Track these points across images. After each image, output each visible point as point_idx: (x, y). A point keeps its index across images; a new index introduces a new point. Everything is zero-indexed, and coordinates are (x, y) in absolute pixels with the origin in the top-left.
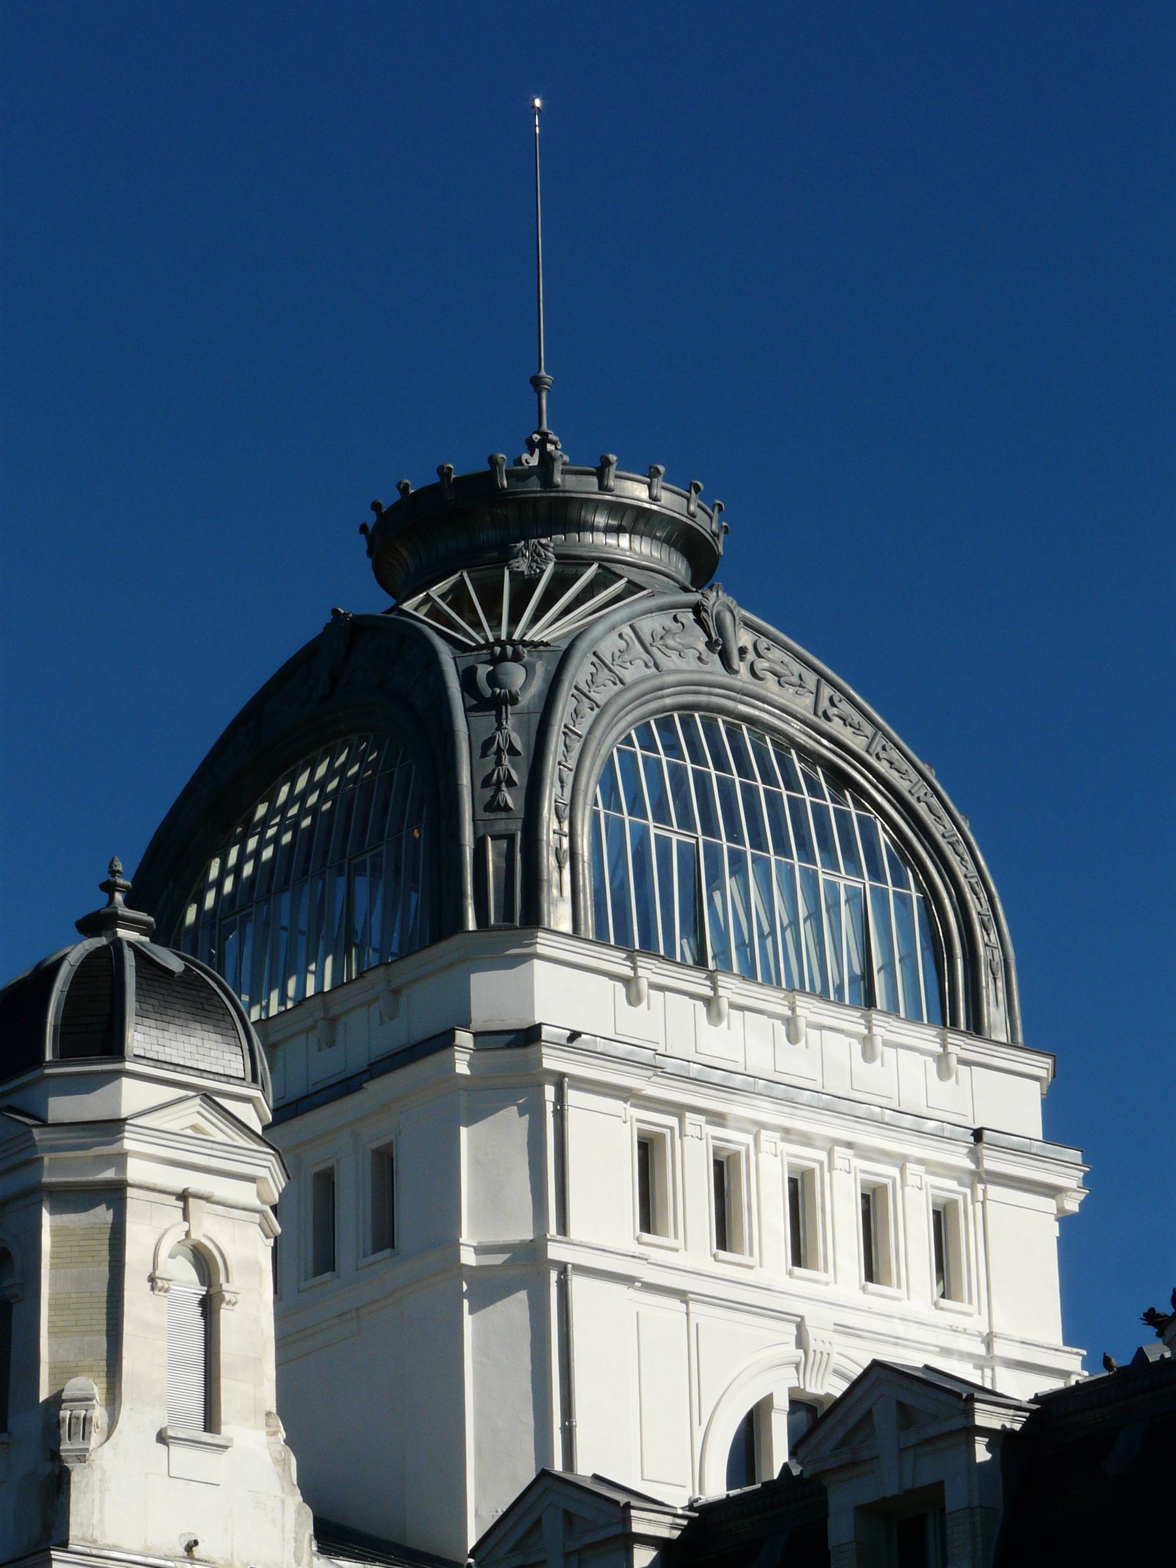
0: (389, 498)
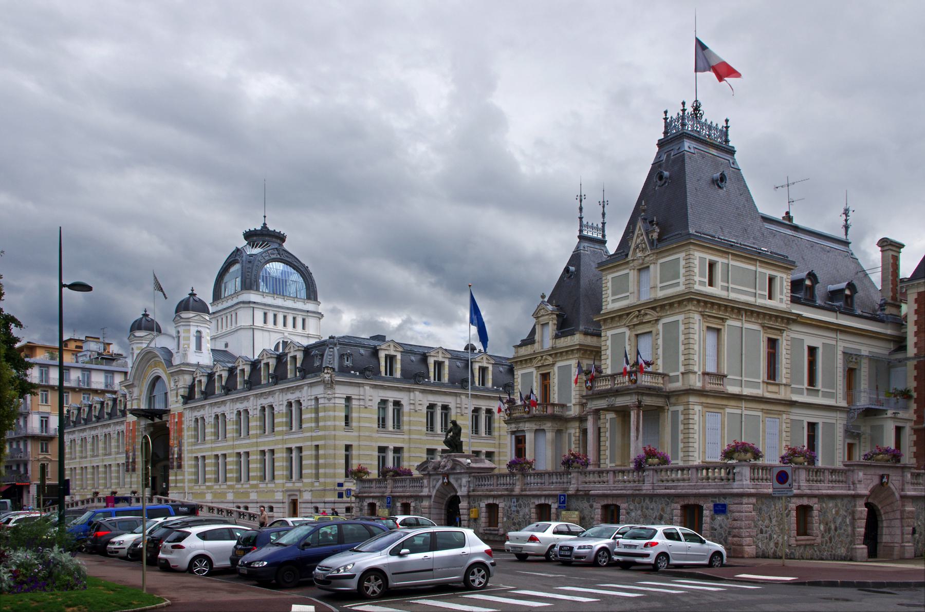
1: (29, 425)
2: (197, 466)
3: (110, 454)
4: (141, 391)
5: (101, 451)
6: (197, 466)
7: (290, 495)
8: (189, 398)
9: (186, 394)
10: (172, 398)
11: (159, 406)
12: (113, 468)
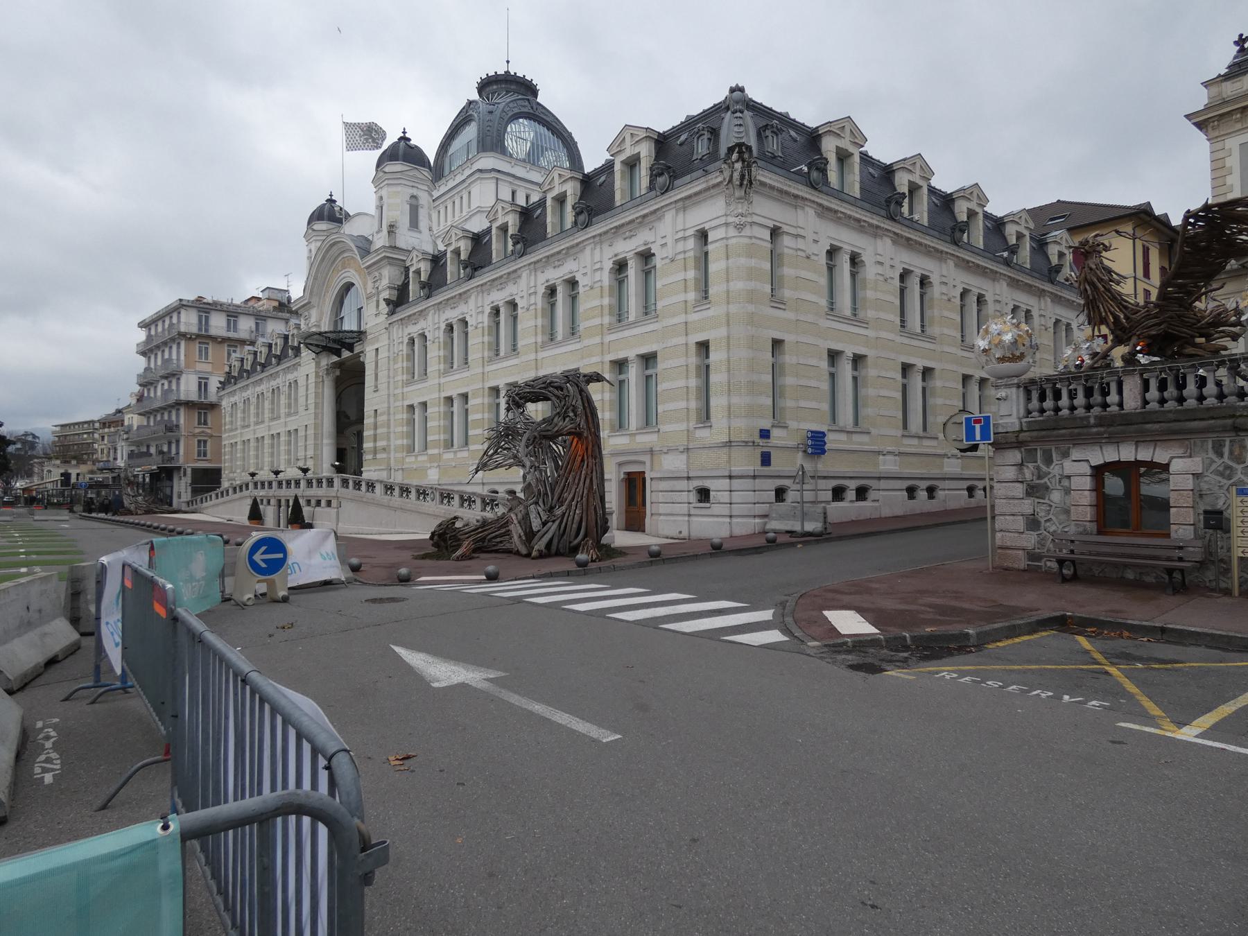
0: (484, 76)
1: (182, 388)
2: (411, 422)
3: (278, 418)
4: (321, 314)
5: (283, 411)
6: (411, 422)
7: (620, 465)
8: (399, 300)
9: (394, 298)
10: (369, 311)
11: (349, 325)
12: (282, 438)
